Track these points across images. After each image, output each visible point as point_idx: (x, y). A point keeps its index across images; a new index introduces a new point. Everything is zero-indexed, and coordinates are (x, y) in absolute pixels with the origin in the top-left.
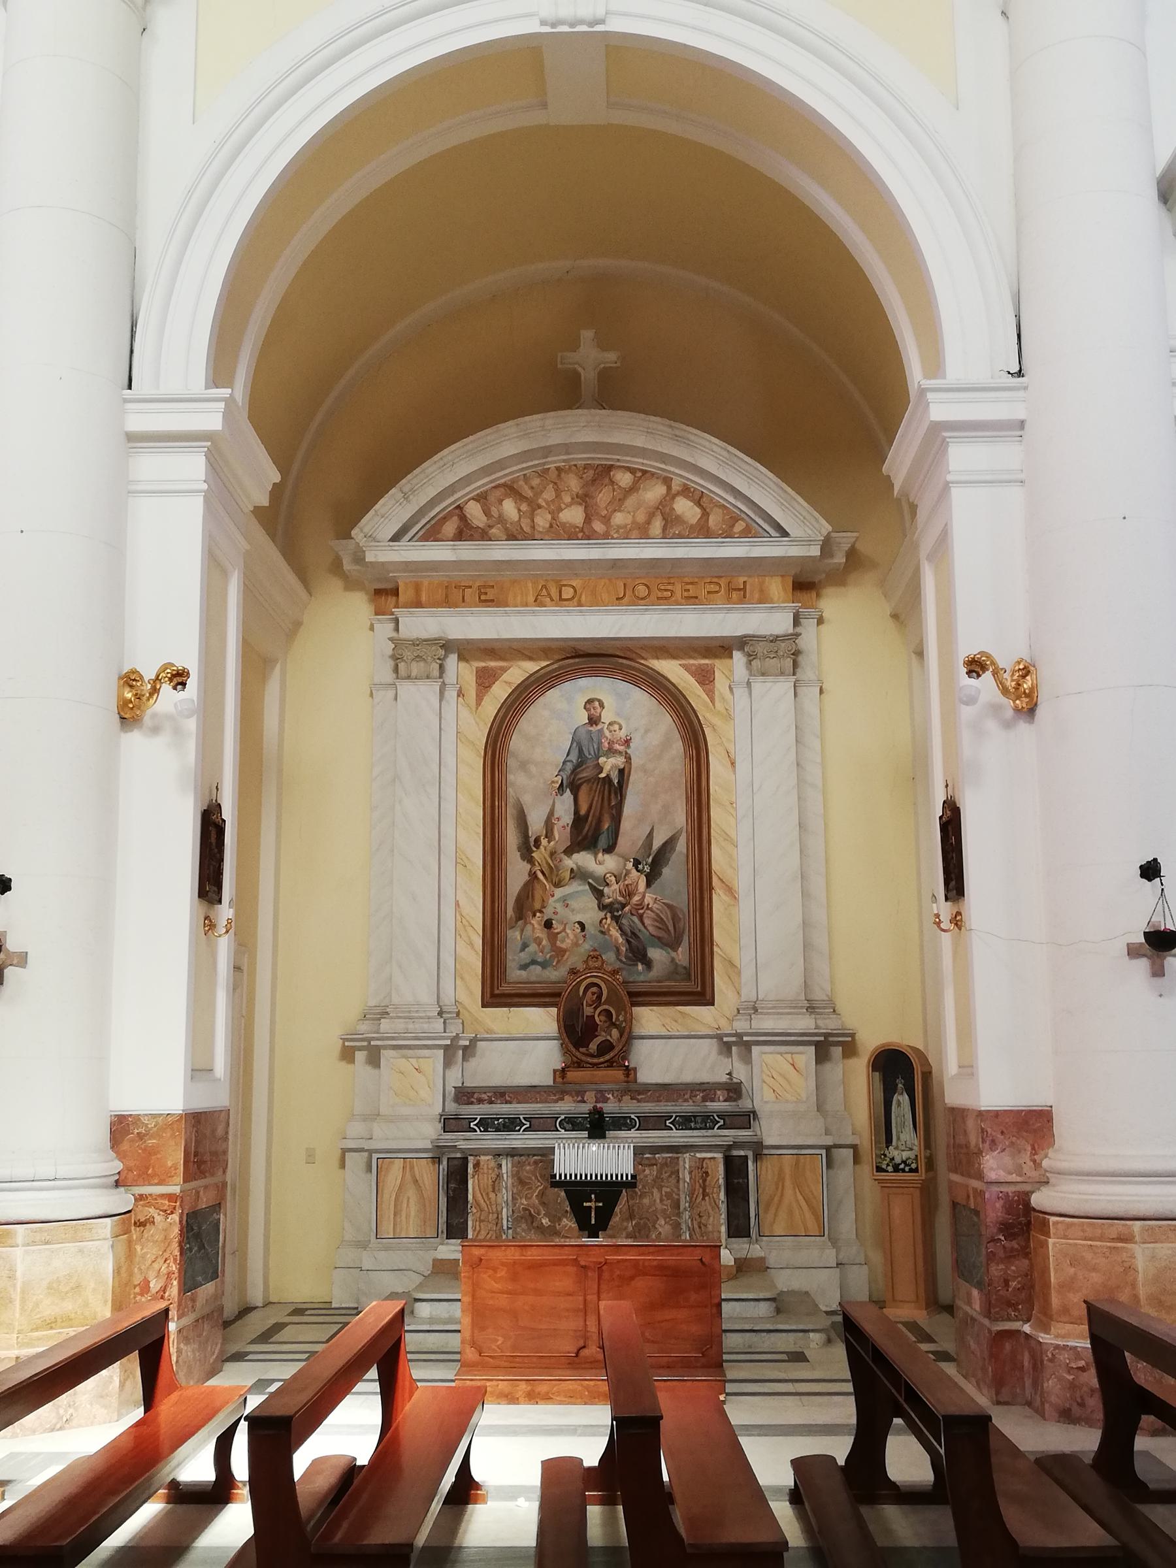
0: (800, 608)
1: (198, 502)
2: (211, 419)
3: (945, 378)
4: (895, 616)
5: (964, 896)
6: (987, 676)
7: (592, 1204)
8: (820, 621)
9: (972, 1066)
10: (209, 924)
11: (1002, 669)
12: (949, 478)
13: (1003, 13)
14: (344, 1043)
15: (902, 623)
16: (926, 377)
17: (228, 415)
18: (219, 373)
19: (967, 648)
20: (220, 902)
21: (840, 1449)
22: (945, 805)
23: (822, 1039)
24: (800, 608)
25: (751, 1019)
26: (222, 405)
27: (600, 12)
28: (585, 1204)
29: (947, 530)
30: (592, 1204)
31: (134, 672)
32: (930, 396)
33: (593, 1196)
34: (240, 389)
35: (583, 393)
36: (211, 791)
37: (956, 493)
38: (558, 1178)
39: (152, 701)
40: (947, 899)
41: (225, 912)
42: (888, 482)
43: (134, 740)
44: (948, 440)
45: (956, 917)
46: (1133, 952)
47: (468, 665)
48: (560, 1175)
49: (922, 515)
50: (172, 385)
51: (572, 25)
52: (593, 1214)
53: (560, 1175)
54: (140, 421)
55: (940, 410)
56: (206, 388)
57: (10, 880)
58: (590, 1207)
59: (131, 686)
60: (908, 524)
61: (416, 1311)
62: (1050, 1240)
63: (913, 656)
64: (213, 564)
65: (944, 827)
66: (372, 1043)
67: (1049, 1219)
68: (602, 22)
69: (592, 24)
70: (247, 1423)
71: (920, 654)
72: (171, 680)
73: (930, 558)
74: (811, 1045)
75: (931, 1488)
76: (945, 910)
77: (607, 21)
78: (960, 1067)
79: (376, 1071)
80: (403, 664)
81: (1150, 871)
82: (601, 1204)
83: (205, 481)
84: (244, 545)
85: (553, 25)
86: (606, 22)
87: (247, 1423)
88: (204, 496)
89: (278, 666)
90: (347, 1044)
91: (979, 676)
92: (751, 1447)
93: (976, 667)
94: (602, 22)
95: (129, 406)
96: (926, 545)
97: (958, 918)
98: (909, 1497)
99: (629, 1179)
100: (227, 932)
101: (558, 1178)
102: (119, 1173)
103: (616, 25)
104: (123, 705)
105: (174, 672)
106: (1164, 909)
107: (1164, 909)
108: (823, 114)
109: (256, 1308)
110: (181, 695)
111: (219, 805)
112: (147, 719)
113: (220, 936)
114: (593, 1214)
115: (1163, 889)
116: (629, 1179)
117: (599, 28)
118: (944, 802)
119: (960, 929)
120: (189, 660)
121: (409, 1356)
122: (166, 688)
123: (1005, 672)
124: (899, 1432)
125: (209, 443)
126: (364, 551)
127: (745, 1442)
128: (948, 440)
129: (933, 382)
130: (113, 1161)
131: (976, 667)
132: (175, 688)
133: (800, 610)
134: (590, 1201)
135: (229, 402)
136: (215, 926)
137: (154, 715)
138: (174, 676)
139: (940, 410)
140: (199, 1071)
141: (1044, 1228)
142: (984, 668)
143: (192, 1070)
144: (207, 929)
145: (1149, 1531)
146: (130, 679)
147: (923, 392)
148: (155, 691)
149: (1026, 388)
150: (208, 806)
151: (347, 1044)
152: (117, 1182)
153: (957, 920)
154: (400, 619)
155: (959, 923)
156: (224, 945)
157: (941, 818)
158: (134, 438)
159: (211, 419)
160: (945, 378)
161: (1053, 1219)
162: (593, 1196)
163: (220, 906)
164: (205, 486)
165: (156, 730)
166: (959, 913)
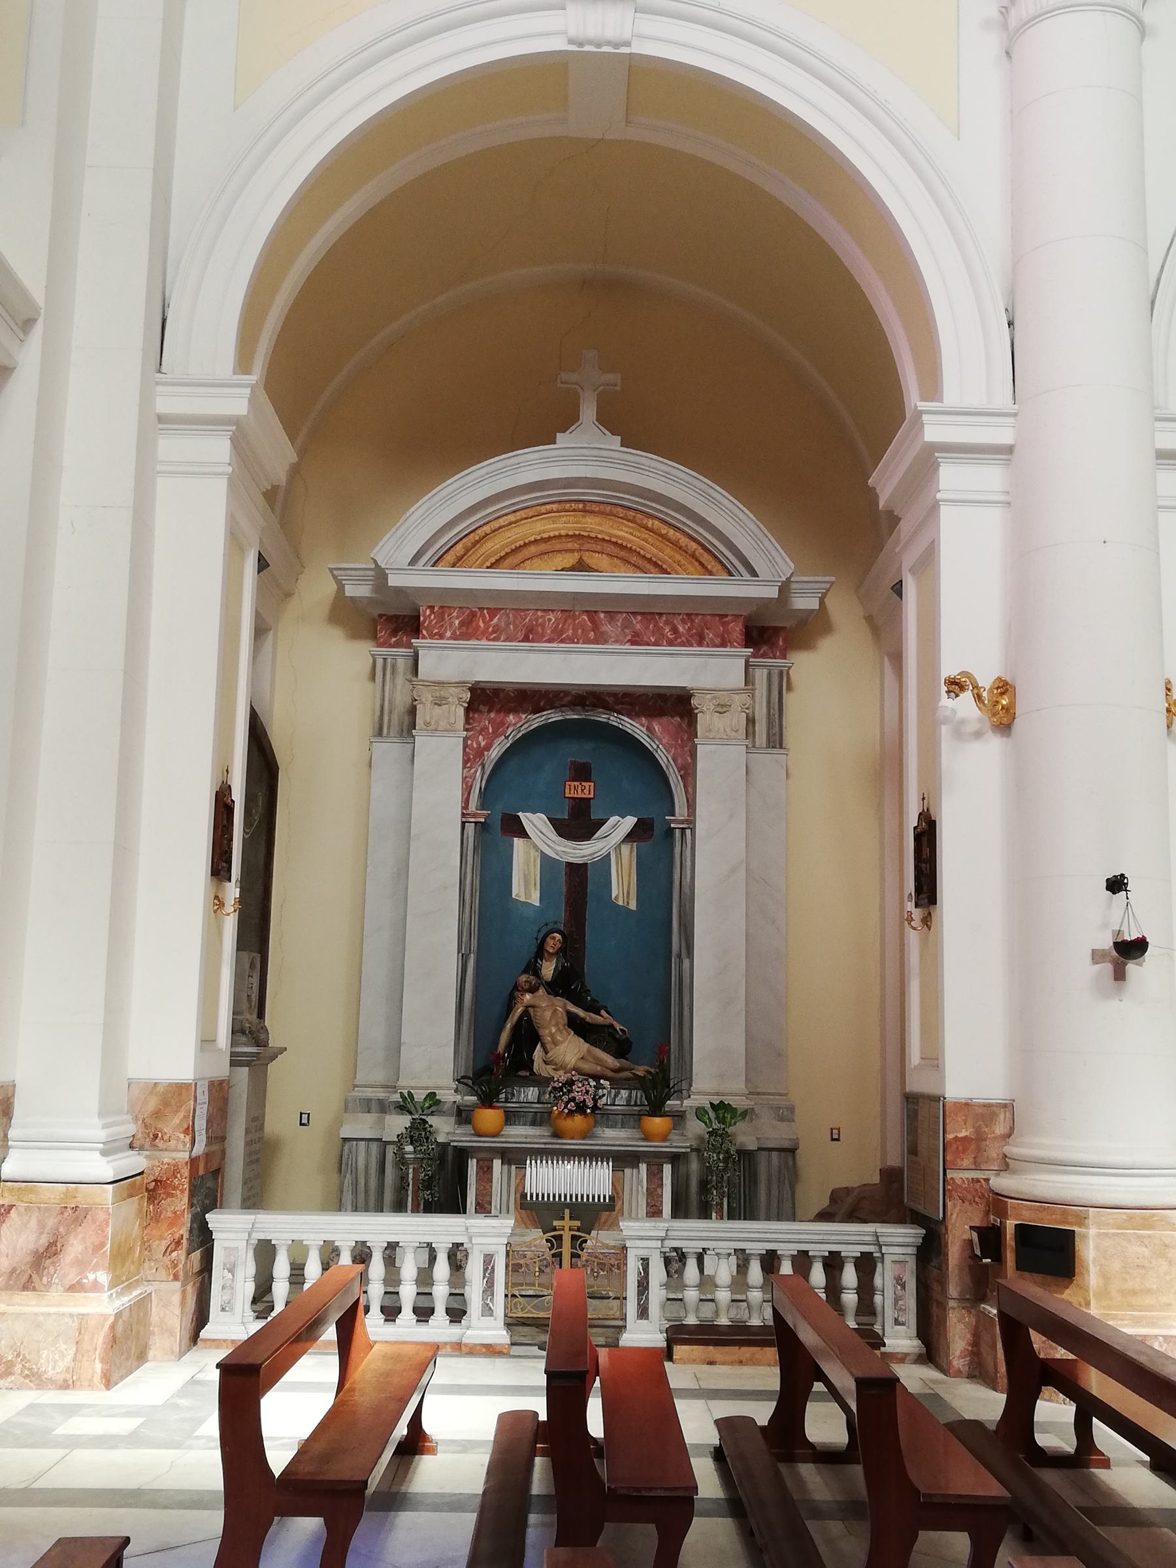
1: (222, 485)
2: (237, 403)
5: (936, 904)
6: (967, 696)
9: (937, 1059)
12: (939, 496)
13: (1007, 53)
16: (923, 399)
17: (252, 400)
18: (243, 363)
19: (949, 669)
21: (763, 1413)
26: (248, 391)
27: (626, 35)
32: (925, 417)
34: (253, 378)
35: (595, 403)
36: (223, 772)
37: (945, 512)
38: (529, 1199)
46: (1097, 956)
47: (932, 813)
49: (905, 527)
54: (168, 403)
55: (934, 431)
56: (235, 373)
68: (627, 44)
69: (617, 45)
70: (219, 1370)
71: (897, 658)
75: (844, 1449)
76: (917, 914)
80: (421, 705)
81: (1116, 885)
83: (229, 464)
87: (219, 1370)
91: (957, 696)
92: (683, 1407)
93: (955, 686)
98: (826, 1457)
101: (529, 1199)
102: (133, 1136)
103: (638, 48)
106: (1123, 919)
107: (1123, 919)
111: (230, 786)
117: (624, 50)
118: (920, 814)
121: (159, 468)
124: (820, 1397)
125: (235, 428)
126: (387, 575)
127: (680, 1405)
131: (955, 686)
139: (934, 431)
142: (962, 688)
143: (202, 1041)
145: (1040, 1489)
147: (919, 414)
154: (420, 652)
157: (915, 828)
163: (228, 884)
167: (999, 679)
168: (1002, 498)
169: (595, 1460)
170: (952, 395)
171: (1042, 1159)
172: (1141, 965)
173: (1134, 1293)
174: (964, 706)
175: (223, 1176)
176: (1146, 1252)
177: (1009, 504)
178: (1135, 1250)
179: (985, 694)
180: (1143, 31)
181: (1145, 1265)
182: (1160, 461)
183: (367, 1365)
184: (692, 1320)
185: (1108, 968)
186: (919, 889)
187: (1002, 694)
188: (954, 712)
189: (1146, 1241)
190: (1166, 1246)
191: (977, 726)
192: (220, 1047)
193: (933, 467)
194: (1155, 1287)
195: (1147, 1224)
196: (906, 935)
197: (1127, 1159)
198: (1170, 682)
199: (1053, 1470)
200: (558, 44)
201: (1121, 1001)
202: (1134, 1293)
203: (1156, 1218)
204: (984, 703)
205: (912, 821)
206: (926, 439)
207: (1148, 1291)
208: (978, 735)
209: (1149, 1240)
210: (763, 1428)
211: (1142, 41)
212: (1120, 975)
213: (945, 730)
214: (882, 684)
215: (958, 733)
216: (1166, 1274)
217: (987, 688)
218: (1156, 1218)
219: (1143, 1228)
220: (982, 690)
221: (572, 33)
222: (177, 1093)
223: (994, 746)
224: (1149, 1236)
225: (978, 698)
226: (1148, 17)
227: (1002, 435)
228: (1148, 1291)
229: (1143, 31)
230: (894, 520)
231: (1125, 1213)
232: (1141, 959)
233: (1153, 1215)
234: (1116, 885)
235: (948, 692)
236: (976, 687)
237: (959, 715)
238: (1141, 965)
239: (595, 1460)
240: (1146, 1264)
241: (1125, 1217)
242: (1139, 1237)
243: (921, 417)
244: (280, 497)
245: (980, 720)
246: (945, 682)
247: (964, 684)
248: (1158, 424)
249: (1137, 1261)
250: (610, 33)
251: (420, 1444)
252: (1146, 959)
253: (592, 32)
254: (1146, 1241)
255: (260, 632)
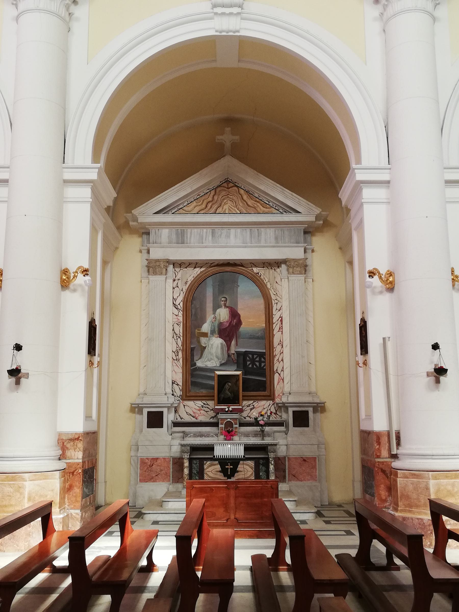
0: (307, 246)
1: (88, 206)
2: (93, 175)
3: (361, 164)
4: (340, 248)
5: (368, 353)
6: (376, 277)
7: (229, 467)
8: (313, 251)
10: (91, 363)
11: (381, 274)
12: (363, 201)
14: (131, 405)
15: (343, 251)
17: (99, 174)
18: (96, 159)
19: (369, 267)
20: (95, 355)
22: (362, 320)
23: (316, 405)
24: (307, 246)
25: (288, 397)
26: (97, 170)
27: (238, 28)
28: (229, 474)
29: (362, 221)
30: (229, 467)
31: (67, 269)
32: (356, 171)
33: (229, 464)
34: (101, 164)
37: (365, 206)
38: (216, 457)
39: (74, 280)
40: (361, 354)
41: (96, 359)
42: (340, 201)
43: (67, 294)
44: (363, 187)
45: (364, 362)
46: (428, 375)
48: (217, 456)
49: (352, 213)
50: (79, 162)
51: (227, 32)
52: (229, 470)
53: (217, 456)
54: (68, 175)
55: (360, 176)
57: (22, 346)
58: (228, 468)
59: (65, 274)
60: (345, 216)
61: (163, 505)
62: (398, 479)
63: (347, 264)
64: (94, 229)
65: (361, 328)
66: (140, 406)
67: (397, 471)
68: (238, 31)
71: (351, 263)
72: (82, 272)
73: (356, 229)
74: (311, 407)
75: (386, 565)
76: (360, 359)
77: (240, 31)
78: (366, 416)
79: (142, 416)
81: (435, 347)
82: (232, 467)
84: (104, 221)
85: (221, 32)
86: (240, 32)
88: (91, 204)
89: (110, 265)
90: (133, 406)
93: (372, 274)
94: (238, 31)
95: (6, 199)
96: (354, 225)
97: (366, 362)
99: (242, 457)
100: (98, 366)
101: (216, 457)
102: (60, 455)
104: (62, 281)
105: (84, 270)
108: (345, 99)
109: (101, 506)
110: (87, 278)
111: (95, 319)
112: (71, 286)
113: (95, 368)
114: (229, 470)
115: (440, 354)
116: (242, 457)
118: (361, 319)
119: (366, 366)
120: (86, 266)
122: (80, 276)
123: (382, 275)
125: (92, 184)
128: (363, 187)
129: (358, 166)
130: (58, 450)
131: (372, 274)
132: (84, 276)
133: (307, 247)
134: (228, 465)
135: (99, 169)
136: (93, 364)
137: (74, 285)
138: (84, 271)
139: (360, 176)
140: (88, 417)
141: (396, 475)
142: (375, 274)
143: (86, 417)
144: (90, 365)
146: (65, 272)
148: (75, 277)
149: (390, 169)
150: (91, 320)
151: (133, 406)
152: (59, 458)
153: (365, 363)
155: (366, 364)
156: (96, 371)
158: (66, 182)
159: (93, 175)
160: (361, 164)
161: (398, 471)
162: (229, 464)
163: (95, 357)
164: (91, 200)
165: (75, 290)
166: (366, 360)
167: (388, 271)
168: (386, 201)
169: (271, 572)
170: (365, 163)
171: (415, 454)
172: (446, 377)
173: (6, 506)
174: (376, 280)
175: (96, 469)
176: (12, 490)
177: (389, 203)
178: (8, 490)
179: (383, 276)
180: (434, 19)
181: (11, 495)
182: (446, 184)
183: (129, 540)
184: (65, 521)
185: (433, 379)
186: (362, 348)
187: (390, 276)
188: (372, 283)
189: (12, 486)
190: (20, 487)
191: (380, 289)
192: (94, 419)
193: (361, 189)
194: (14, 503)
195: (13, 479)
196: (358, 369)
197: (11, 454)
198: (453, 268)
199: (380, 572)
200: (212, 33)
201: (439, 391)
202: (6, 506)
203: (17, 477)
204: (383, 280)
205: (358, 322)
206: (357, 179)
207: (11, 505)
208: (381, 292)
209: (13, 485)
210: (268, 558)
211: (434, 23)
212: (438, 381)
213: (368, 290)
214: (346, 274)
215: (374, 293)
216: (19, 498)
217: (384, 274)
218: (17, 477)
219: (12, 480)
220: (381, 275)
221: (217, 28)
222: (75, 439)
223: (387, 296)
224: (13, 484)
225: (380, 278)
226: (437, 13)
227: (385, 177)
228: (11, 505)
229: (434, 19)
230: (348, 211)
231: (5, 475)
232: (446, 374)
233: (16, 476)
234: (435, 347)
235: (369, 276)
236: (379, 273)
237: (374, 285)
238: (446, 377)
239: (271, 572)
240: (11, 495)
241: (5, 477)
242: (9, 484)
243: (354, 170)
244: (111, 210)
245: (381, 287)
246: (368, 273)
247: (375, 272)
248: (445, 170)
249: (8, 494)
250: (232, 28)
251: (152, 568)
252: (448, 374)
253: (225, 27)
254: (12, 486)
255: (105, 263)
